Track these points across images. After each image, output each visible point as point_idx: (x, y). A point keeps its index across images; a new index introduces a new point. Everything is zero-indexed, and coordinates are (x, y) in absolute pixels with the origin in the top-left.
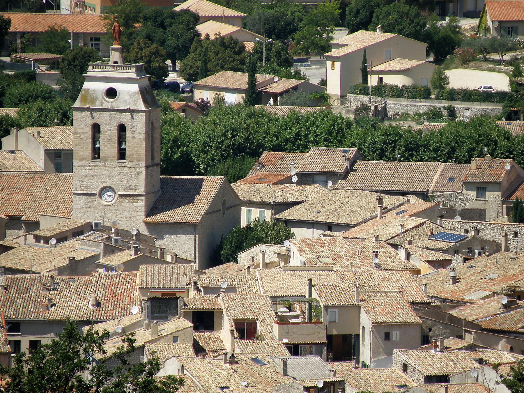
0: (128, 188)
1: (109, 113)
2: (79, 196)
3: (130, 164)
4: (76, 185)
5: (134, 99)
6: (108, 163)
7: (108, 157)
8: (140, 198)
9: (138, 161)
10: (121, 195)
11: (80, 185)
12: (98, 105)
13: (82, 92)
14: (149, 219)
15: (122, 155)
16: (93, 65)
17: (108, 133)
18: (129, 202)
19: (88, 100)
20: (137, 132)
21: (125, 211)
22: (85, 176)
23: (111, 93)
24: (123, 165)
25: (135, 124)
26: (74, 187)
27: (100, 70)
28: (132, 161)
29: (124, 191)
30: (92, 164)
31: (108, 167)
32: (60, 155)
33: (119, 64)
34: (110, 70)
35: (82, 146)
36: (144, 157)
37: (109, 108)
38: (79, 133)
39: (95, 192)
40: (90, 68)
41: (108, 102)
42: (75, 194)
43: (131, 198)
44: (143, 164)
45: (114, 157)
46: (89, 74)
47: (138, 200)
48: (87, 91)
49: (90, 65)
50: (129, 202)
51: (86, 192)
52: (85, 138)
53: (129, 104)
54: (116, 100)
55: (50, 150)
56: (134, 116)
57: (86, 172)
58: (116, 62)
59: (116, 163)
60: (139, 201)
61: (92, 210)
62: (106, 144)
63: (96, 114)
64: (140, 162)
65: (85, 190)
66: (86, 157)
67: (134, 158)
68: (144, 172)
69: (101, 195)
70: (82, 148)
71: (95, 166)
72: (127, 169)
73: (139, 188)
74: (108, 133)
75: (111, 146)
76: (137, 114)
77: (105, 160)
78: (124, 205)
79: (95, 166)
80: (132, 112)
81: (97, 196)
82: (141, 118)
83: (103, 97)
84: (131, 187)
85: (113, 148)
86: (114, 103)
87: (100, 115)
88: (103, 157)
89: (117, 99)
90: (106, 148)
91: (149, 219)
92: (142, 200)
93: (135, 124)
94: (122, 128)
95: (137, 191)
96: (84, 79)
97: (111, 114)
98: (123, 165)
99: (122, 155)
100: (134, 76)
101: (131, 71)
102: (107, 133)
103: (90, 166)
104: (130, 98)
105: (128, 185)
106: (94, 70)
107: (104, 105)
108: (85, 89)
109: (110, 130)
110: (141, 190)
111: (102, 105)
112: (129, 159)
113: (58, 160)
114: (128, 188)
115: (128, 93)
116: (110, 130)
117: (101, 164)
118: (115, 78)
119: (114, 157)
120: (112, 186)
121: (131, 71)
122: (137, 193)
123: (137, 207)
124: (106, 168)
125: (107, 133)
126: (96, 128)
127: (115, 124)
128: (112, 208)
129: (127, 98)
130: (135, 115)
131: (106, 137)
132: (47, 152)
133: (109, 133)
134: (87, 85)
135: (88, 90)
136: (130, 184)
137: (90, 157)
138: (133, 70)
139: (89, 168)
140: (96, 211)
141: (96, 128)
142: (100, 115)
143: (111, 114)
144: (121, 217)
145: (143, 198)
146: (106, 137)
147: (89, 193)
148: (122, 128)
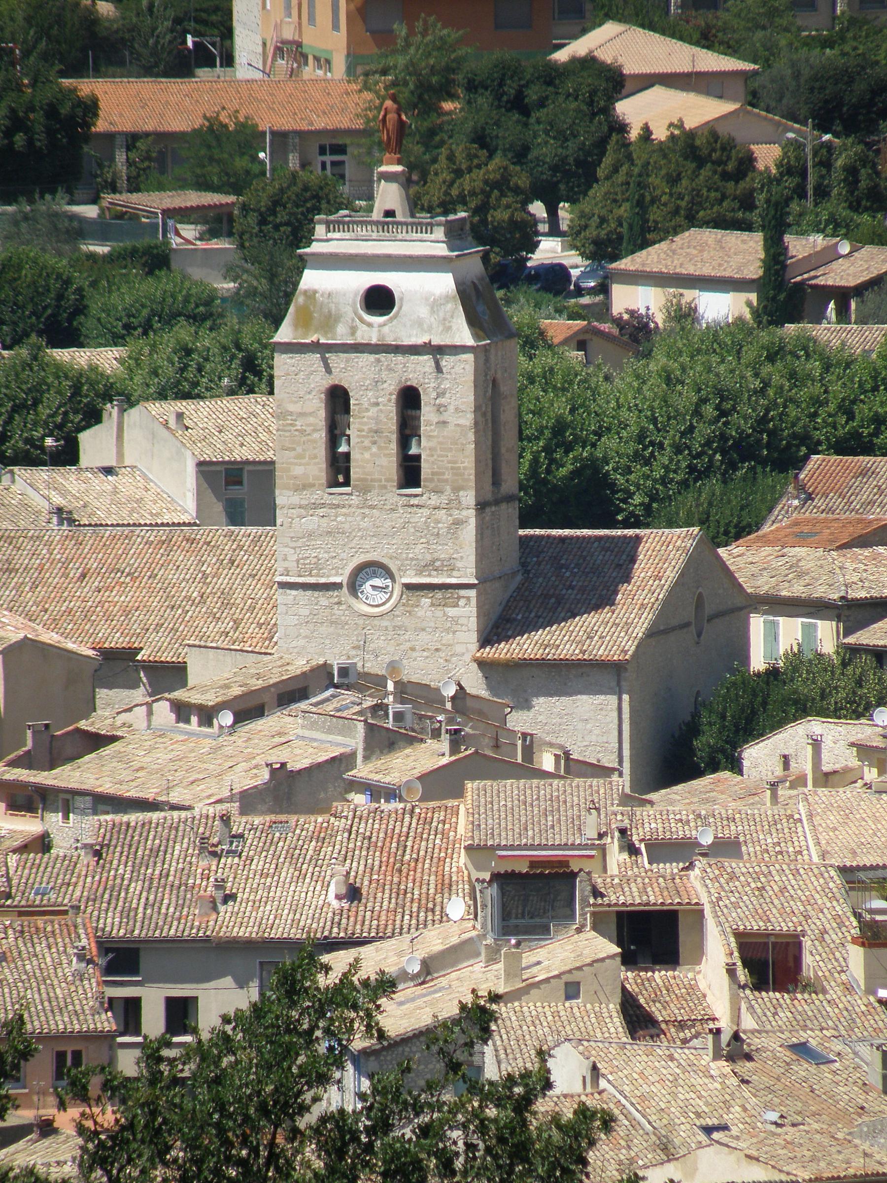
0: (430, 566)
1: (372, 357)
2: (294, 592)
3: (434, 500)
4: (285, 559)
5: (441, 314)
6: (373, 498)
7: (372, 480)
8: (463, 592)
9: (456, 489)
10: (410, 587)
11: (298, 561)
12: (341, 335)
13: (299, 299)
14: (489, 653)
15: (410, 473)
16: (328, 223)
17: (373, 412)
18: (432, 605)
20: (451, 408)
21: (423, 630)
22: (310, 535)
23: (379, 300)
25: (446, 385)
26: (280, 566)
27: (347, 235)
28: (438, 491)
29: (420, 573)
30: (328, 499)
31: (372, 507)
32: (241, 476)
33: (399, 218)
34: (375, 235)
35: (299, 449)
36: (473, 477)
38: (291, 414)
39: (338, 580)
40: (320, 230)
41: (370, 325)
42: (283, 585)
43: (439, 595)
44: (469, 498)
45: (387, 480)
46: (316, 248)
47: (459, 598)
48: (311, 295)
49: (320, 222)
50: (432, 605)
51: (312, 580)
52: (309, 429)
53: (430, 330)
54: (391, 319)
55: (211, 463)
57: (311, 522)
58: (390, 213)
59: (394, 496)
60: (462, 602)
61: (331, 630)
62: (367, 443)
63: (337, 360)
64: (461, 493)
65: (310, 575)
67: (446, 481)
68: (473, 521)
69: (354, 587)
70: (300, 456)
71: (338, 506)
72: (426, 512)
73: (459, 564)
74: (373, 412)
75: (380, 448)
76: (452, 358)
77: (365, 490)
79: (338, 506)
80: (437, 351)
81: (345, 589)
83: (356, 313)
84: (438, 564)
85: (385, 455)
86: (386, 329)
87: (347, 361)
89: (395, 317)
90: (367, 455)
91: (489, 653)
93: (446, 385)
94: (409, 399)
95: (455, 573)
96: (302, 263)
97: (378, 361)
99: (410, 473)
100: (441, 250)
101: (433, 237)
102: (370, 414)
103: (316, 506)
104: (432, 312)
105: (429, 557)
106: (330, 235)
107: (359, 334)
108: (305, 292)
109: (377, 404)
110: (466, 571)
112: (431, 486)
113: (235, 492)
114: (430, 566)
115: (427, 299)
116: (377, 404)
117: (355, 500)
118: (389, 257)
119: (387, 480)
120: (385, 561)
121: (433, 237)
122: (454, 581)
123: (455, 620)
124: (367, 511)
125: (370, 414)
126: (338, 400)
127: (391, 387)
128: (385, 623)
129: (423, 312)
130: (447, 362)
131: (366, 424)
132: (204, 468)
133: (373, 411)
134: (312, 279)
135: (315, 292)
136: (436, 555)
137: (323, 481)
138: (439, 233)
139: (321, 512)
140: (341, 632)
141: (338, 400)
142: (347, 361)
145: (472, 593)
146: (366, 424)
147: (323, 580)
148: (409, 399)
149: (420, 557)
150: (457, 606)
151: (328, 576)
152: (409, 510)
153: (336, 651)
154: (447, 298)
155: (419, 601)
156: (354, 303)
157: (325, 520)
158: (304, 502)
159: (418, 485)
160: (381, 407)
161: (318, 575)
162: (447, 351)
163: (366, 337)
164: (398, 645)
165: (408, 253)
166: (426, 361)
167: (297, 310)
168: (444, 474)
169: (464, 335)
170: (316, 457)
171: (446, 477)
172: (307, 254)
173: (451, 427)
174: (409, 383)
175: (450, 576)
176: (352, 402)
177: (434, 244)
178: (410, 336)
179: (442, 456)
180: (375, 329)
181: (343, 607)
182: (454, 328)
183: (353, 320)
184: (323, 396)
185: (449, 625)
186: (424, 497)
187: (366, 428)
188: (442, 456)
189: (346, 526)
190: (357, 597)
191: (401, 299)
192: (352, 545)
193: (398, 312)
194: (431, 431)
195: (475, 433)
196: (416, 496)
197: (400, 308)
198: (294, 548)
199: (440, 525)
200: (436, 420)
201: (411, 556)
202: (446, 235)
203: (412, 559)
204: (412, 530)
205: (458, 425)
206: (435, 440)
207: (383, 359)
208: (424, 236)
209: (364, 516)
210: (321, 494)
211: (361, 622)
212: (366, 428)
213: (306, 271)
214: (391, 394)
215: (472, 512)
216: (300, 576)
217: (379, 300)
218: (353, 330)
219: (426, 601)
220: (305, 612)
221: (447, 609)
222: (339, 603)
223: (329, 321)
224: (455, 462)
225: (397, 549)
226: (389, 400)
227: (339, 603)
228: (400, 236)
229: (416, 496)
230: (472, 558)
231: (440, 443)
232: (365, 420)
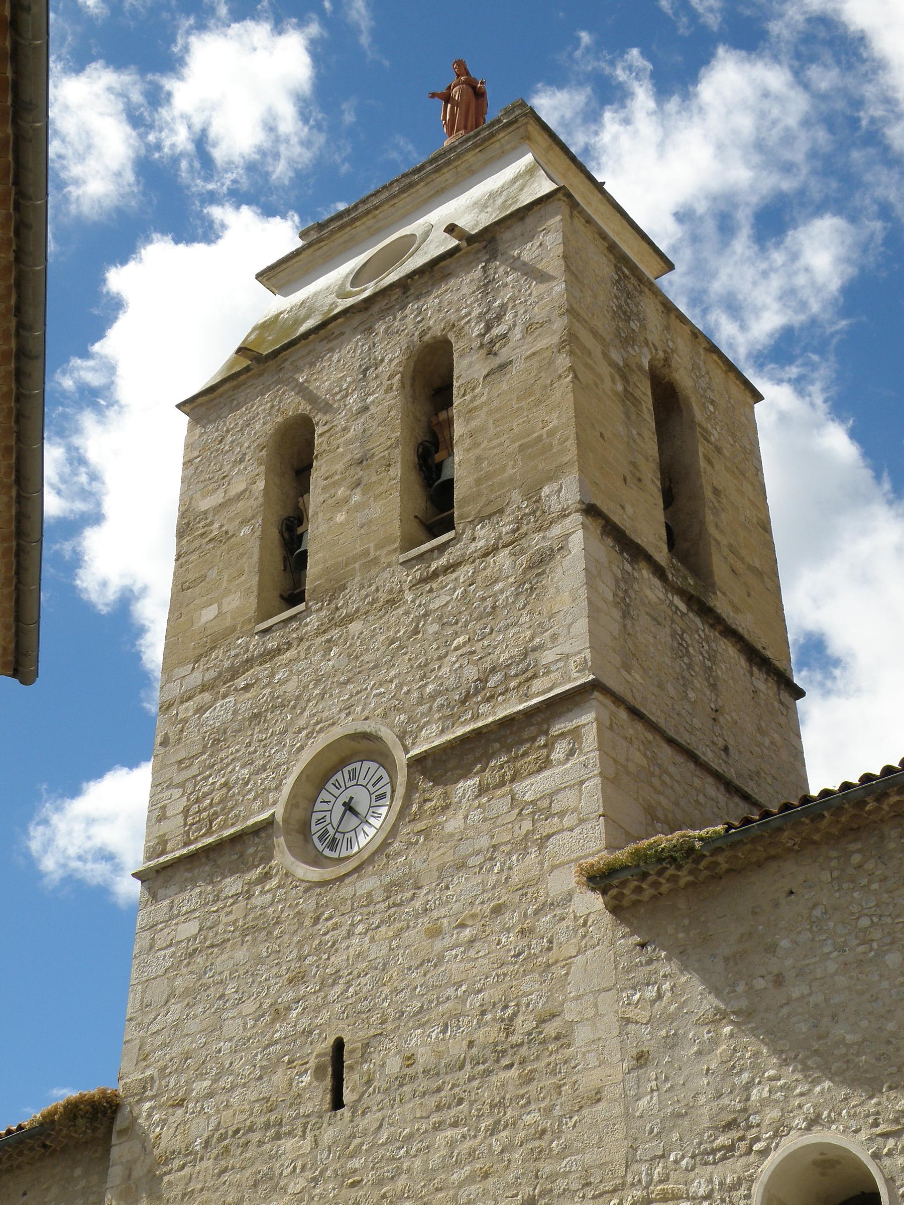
68: (577, 540)
118: (415, 272)
144: (435, 932)
149: (451, 682)
153: (249, 1007)
164: (398, 935)
168: (504, 468)
170: (352, 1051)
185: (527, 825)
198: (182, 785)
211: (308, 905)
221: (519, 787)
230: (582, 625)
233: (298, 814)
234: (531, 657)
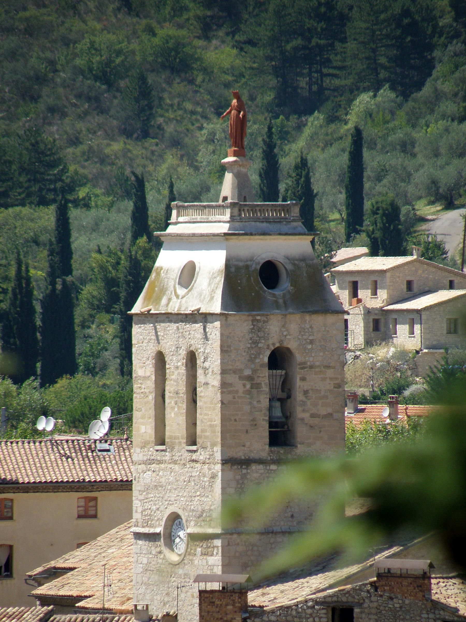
1: (174, 326)
9: (213, 445)
10: (193, 537)
11: (142, 512)
16: (178, 207)
19: (155, 295)
20: (210, 370)
23: (188, 274)
24: (194, 457)
28: (204, 448)
31: (175, 462)
34: (199, 218)
37: (176, 311)
39: (158, 530)
46: (171, 229)
47: (214, 547)
50: (202, 554)
51: (146, 530)
56: (207, 330)
58: (225, 199)
59: (182, 451)
66: (148, 439)
67: (206, 437)
68: (220, 474)
69: (170, 540)
70: (143, 417)
72: (198, 465)
78: (196, 562)
79: (160, 462)
81: (162, 539)
82: (214, 329)
88: (171, 437)
92: (217, 547)
94: (192, 359)
98: (194, 457)
102: (173, 377)
106: (181, 219)
111: (167, 305)
116: (177, 368)
118: (194, 235)
120: (180, 512)
124: (172, 466)
126: (160, 360)
127: (183, 352)
135: (161, 268)
137: (153, 439)
141: (160, 360)
143: (178, 328)
145: (218, 543)
147: (152, 531)
148: (192, 359)
150: (212, 555)
151: (155, 527)
152: (192, 464)
154: (222, 271)
155: (195, 550)
156: (176, 278)
157: (154, 475)
158: (145, 458)
159: (194, 443)
160: (179, 371)
161: (151, 526)
162: (209, 318)
163: (173, 309)
165: (179, 232)
166: (199, 326)
167: (149, 286)
169: (216, 307)
170: (150, 418)
171: (208, 434)
172: (161, 235)
173: (210, 388)
174: (191, 349)
175: (210, 527)
176: (167, 366)
177: (220, 224)
178: (192, 306)
179: (206, 414)
180: (179, 300)
181: (162, 556)
182: (215, 298)
183: (171, 293)
184: (154, 361)
186: (198, 453)
187: (172, 389)
188: (206, 414)
189: (163, 480)
190: (173, 550)
191: (198, 273)
192: (166, 498)
193: (193, 286)
194: (201, 392)
195: (222, 393)
196: (195, 451)
197: (195, 282)
198: (140, 501)
199: (205, 479)
200: (203, 382)
201: (192, 507)
202: (232, 217)
203: (193, 510)
204: (193, 483)
205: (213, 386)
206: (203, 399)
207: (180, 327)
208: (218, 217)
209: (172, 470)
210: (152, 451)
212: (172, 389)
213: (162, 250)
214: (183, 359)
215: (218, 467)
216: (143, 527)
217: (188, 274)
218: (170, 300)
219: (199, 550)
220: (145, 561)
222: (160, 552)
223: (163, 291)
224: (212, 421)
225: (186, 501)
226: (183, 365)
227: (160, 552)
228: (211, 218)
229: (195, 451)
231: (205, 403)
232: (172, 382)
233: (168, 531)
234: (211, 512)
